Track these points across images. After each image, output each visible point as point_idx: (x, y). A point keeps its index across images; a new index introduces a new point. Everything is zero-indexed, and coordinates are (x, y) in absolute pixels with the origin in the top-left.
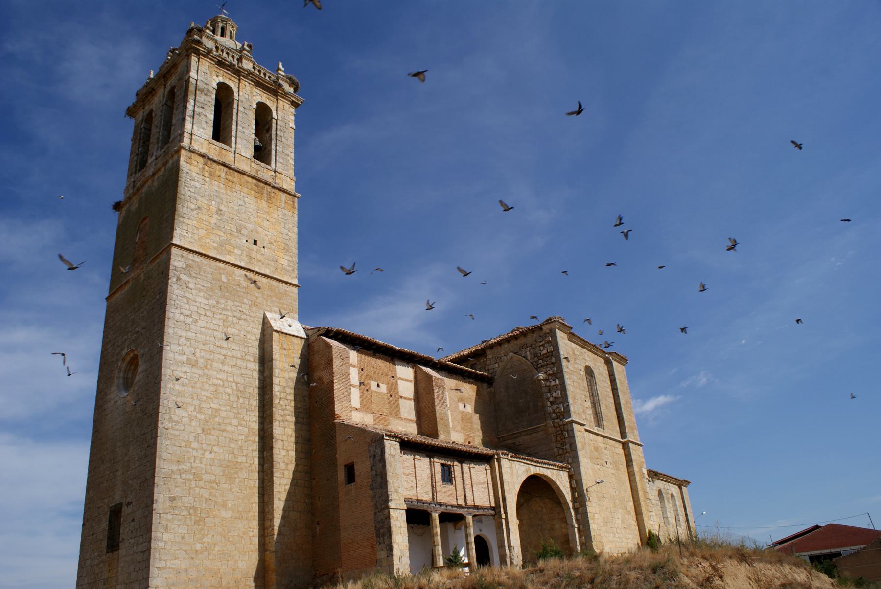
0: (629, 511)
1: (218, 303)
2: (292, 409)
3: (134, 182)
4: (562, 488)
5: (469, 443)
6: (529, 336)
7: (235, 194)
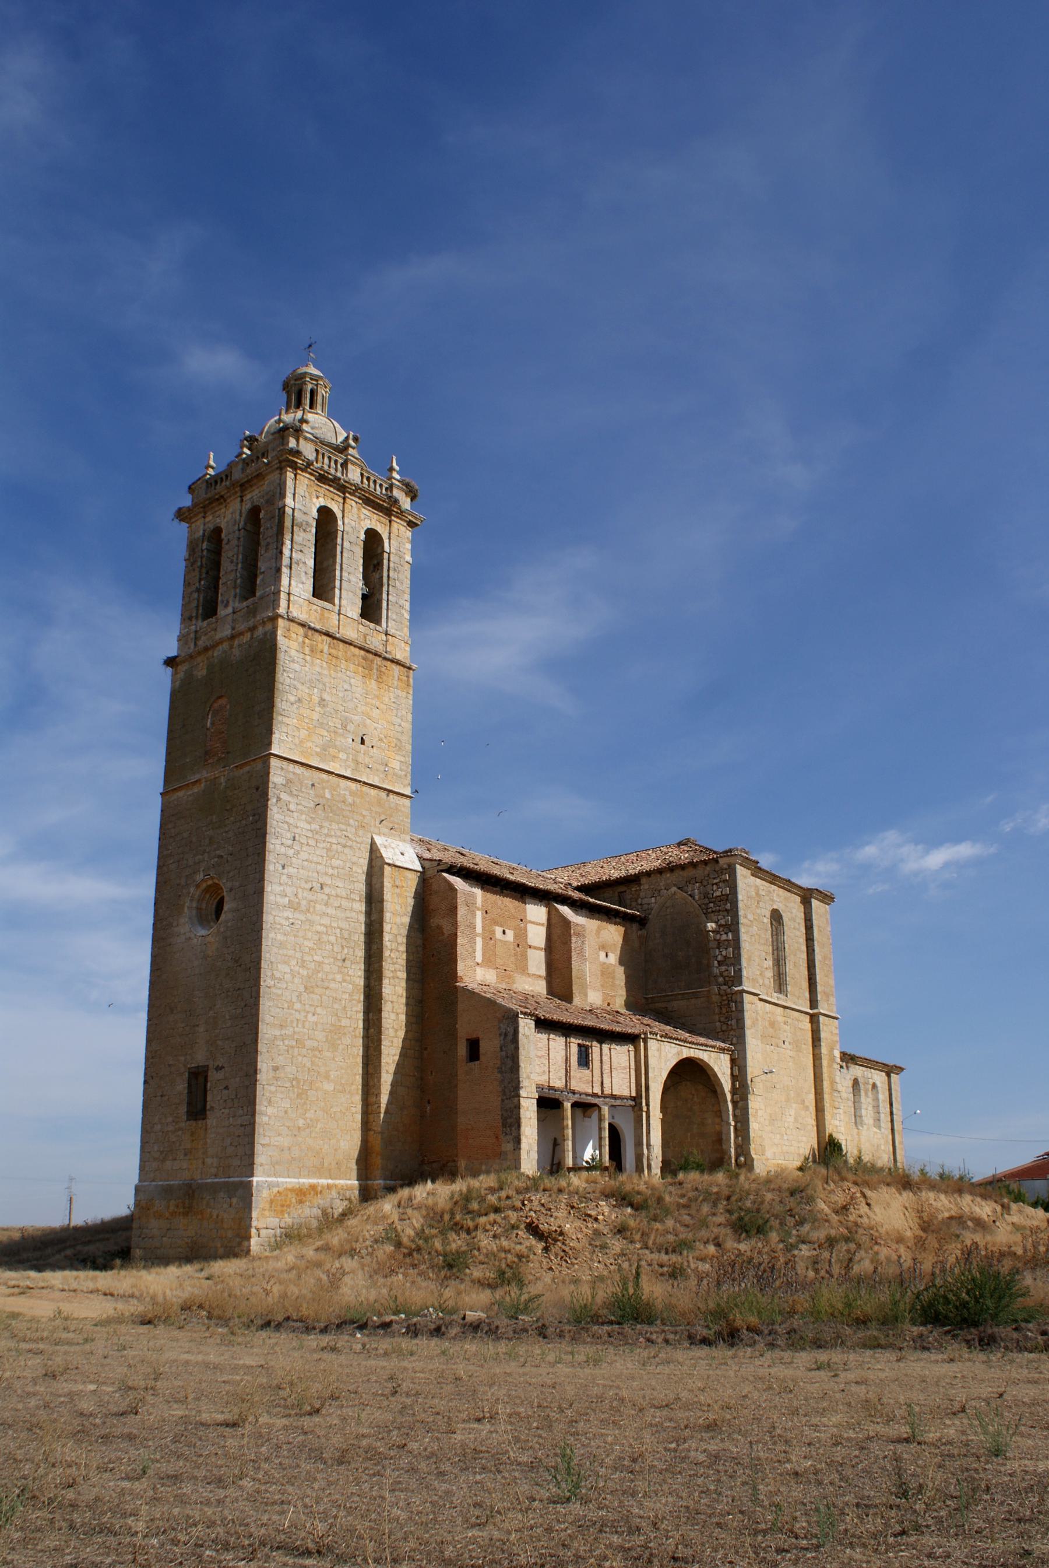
0: (807, 1107)
1: (321, 827)
2: (404, 963)
3: (196, 632)
4: (720, 1075)
5: (609, 1004)
6: (701, 868)
7: (340, 675)
